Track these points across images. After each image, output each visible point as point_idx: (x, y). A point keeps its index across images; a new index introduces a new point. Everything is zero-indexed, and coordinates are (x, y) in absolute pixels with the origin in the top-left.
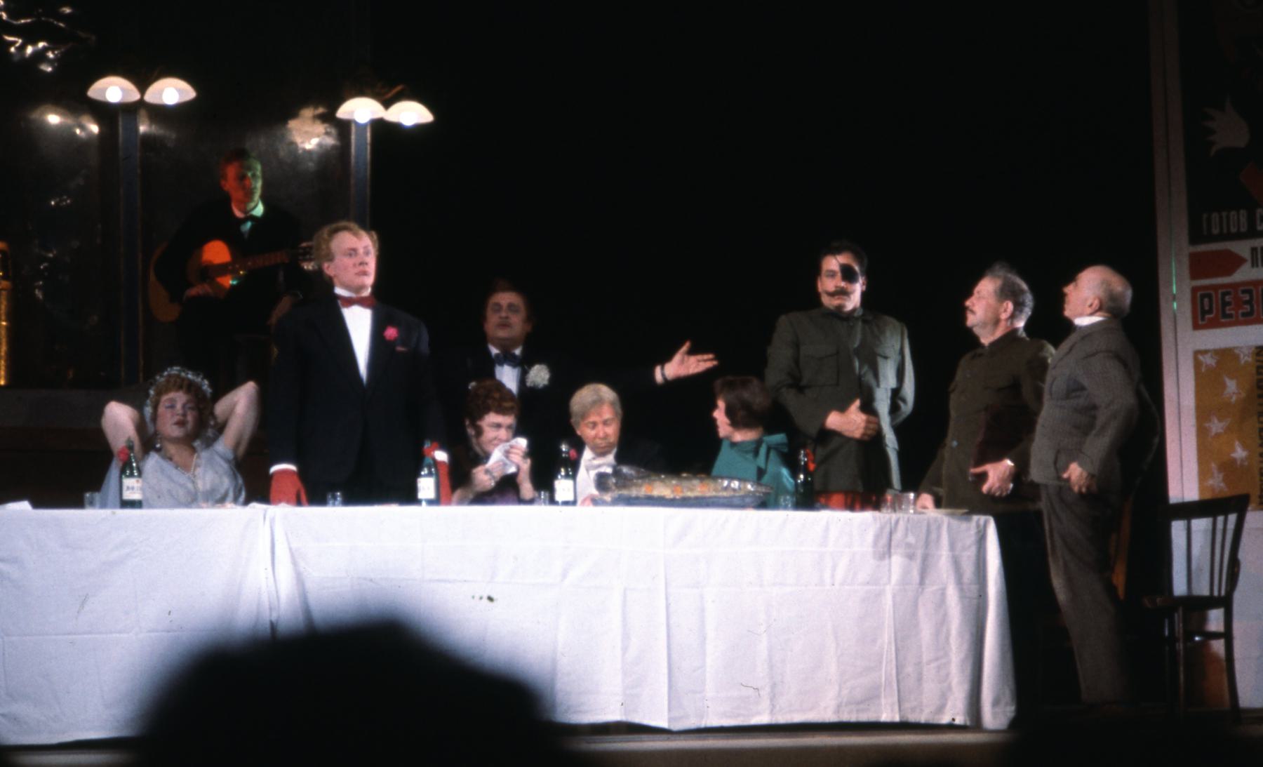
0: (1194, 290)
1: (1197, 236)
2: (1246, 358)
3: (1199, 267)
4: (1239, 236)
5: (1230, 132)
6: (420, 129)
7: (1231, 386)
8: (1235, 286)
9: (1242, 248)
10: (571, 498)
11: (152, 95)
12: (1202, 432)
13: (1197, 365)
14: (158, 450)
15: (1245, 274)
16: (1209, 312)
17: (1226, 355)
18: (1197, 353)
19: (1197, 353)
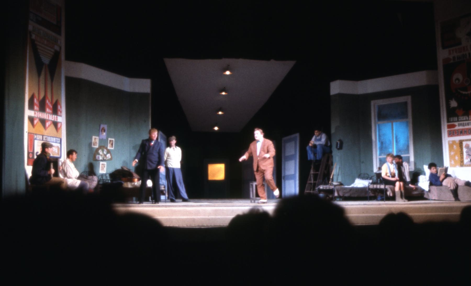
0: (448, 131)
1: (448, 121)
2: (457, 142)
3: (449, 127)
4: (456, 122)
5: (454, 104)
6: (176, 140)
7: (455, 146)
8: (455, 130)
9: (456, 124)
10: (41, 136)
11: (113, 154)
12: (450, 154)
13: (449, 143)
14: (36, 139)
15: (457, 128)
16: (451, 134)
17: (454, 142)
18: (449, 141)
19: (449, 141)
